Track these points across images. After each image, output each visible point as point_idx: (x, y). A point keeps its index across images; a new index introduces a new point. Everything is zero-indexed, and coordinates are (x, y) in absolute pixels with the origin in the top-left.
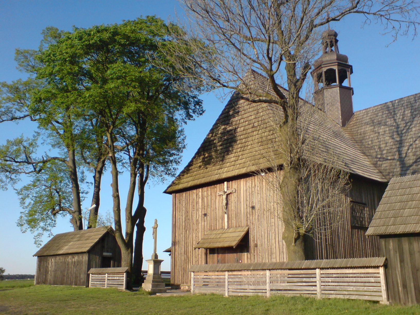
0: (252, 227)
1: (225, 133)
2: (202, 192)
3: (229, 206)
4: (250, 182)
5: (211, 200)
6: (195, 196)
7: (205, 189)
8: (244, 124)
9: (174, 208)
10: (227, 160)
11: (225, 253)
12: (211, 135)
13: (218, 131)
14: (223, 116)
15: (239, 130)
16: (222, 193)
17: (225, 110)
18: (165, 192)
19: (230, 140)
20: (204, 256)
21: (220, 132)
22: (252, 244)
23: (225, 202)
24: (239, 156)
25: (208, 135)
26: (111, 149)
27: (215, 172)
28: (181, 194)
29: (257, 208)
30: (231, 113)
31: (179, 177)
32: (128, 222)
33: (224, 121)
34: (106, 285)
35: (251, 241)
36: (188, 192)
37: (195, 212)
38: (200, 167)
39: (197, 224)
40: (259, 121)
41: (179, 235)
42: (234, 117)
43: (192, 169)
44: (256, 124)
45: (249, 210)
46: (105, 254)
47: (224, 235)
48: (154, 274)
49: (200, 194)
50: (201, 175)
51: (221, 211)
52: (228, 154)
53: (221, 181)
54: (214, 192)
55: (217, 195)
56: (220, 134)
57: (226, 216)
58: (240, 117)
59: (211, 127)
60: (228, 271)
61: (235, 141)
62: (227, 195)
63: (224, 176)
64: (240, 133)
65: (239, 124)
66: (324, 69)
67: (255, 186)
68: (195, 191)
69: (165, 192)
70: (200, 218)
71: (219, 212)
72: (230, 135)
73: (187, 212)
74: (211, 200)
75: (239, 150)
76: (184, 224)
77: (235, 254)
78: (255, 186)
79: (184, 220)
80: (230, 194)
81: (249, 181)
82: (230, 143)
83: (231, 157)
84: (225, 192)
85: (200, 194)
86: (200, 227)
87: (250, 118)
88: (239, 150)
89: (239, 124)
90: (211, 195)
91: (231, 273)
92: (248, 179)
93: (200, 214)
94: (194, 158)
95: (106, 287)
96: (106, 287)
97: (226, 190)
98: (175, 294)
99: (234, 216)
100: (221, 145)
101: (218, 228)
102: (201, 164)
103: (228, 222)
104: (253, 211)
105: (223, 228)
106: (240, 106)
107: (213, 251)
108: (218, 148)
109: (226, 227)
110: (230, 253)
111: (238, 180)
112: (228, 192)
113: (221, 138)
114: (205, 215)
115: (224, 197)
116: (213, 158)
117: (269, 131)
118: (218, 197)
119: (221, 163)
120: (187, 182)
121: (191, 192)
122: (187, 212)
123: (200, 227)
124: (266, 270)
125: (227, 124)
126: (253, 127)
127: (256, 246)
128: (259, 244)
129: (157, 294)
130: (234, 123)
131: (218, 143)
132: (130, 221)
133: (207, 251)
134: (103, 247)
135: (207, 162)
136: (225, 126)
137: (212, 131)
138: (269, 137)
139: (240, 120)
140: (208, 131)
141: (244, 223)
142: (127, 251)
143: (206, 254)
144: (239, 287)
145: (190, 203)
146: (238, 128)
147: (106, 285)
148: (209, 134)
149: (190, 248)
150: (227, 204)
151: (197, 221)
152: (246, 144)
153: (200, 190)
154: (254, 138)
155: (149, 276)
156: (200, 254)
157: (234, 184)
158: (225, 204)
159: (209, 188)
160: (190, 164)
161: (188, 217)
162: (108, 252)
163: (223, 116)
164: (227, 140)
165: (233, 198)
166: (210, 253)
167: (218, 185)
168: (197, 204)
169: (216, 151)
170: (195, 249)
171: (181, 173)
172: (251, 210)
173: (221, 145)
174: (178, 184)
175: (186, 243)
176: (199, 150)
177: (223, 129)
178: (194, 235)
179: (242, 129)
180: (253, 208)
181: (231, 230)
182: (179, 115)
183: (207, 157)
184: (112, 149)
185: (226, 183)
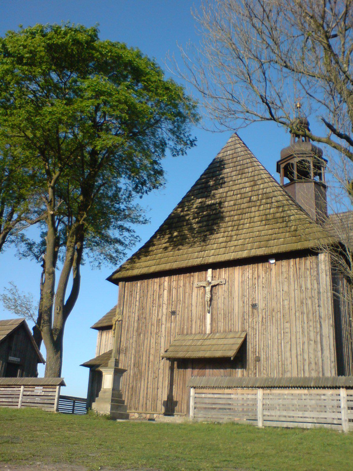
0: (250, 332)
1: (203, 207)
2: (170, 281)
3: (214, 302)
4: (251, 271)
5: (185, 293)
6: (156, 287)
7: (174, 278)
8: (234, 197)
9: (122, 301)
10: (212, 241)
11: (206, 368)
12: (180, 209)
13: (193, 204)
14: (199, 186)
15: (226, 204)
16: (204, 284)
17: (200, 179)
18: (110, 279)
19: (212, 217)
20: (167, 371)
21: (195, 206)
22: (250, 356)
23: (208, 296)
24: (231, 236)
25: (176, 209)
26: (51, 205)
27: (191, 255)
28: (134, 283)
29: (261, 305)
30: (211, 183)
31: (132, 260)
32: (58, 314)
33: (202, 193)
34: (19, 404)
35: (250, 352)
36: (146, 281)
37: (155, 309)
38: (166, 248)
39: (158, 325)
40: (258, 195)
41: (127, 339)
42: (216, 189)
43: (153, 251)
44: (254, 198)
45: (248, 308)
46: (11, 358)
47: (208, 342)
48: (113, 389)
49: (166, 284)
50: (163, 258)
51: (200, 308)
52: (212, 234)
53: (202, 268)
54: (190, 282)
55: (195, 285)
56: (196, 208)
57: (208, 316)
58: (227, 189)
59: (179, 200)
60: (262, 388)
61: (222, 218)
62: (212, 287)
63: (211, 260)
64: (229, 209)
65: (226, 197)
66: (297, 160)
67: (258, 277)
68: (157, 280)
69: (110, 279)
70: (164, 317)
71: (196, 311)
72: (213, 210)
73: (142, 308)
74: (185, 293)
75: (230, 229)
76: (136, 325)
77: (222, 370)
78: (258, 277)
79: (136, 319)
80: (215, 286)
81: (249, 270)
82: (214, 219)
83: (219, 237)
84: (209, 283)
85: (166, 284)
86: (163, 330)
87: (243, 191)
88: (230, 229)
89: (226, 197)
90: (184, 285)
91: (268, 391)
92: (247, 266)
93: (165, 311)
94: (154, 237)
95: (19, 407)
96: (19, 407)
97: (209, 279)
98: (154, 422)
99: (221, 317)
100: (198, 223)
101: (193, 332)
102: (168, 244)
103: (211, 324)
104: (255, 311)
105: (202, 332)
106: (225, 176)
107: (184, 363)
108: (195, 226)
109: (208, 331)
110: (215, 369)
111: (231, 269)
112: (214, 283)
113: (198, 213)
114: (173, 313)
115: (208, 289)
116: (187, 238)
117: (278, 207)
118: (195, 290)
119: (202, 244)
120: (144, 266)
121: (150, 281)
122: (142, 308)
123: (163, 330)
124: (339, 388)
125: (206, 197)
126: (250, 202)
127: (258, 359)
128: (263, 357)
129: (118, 420)
130: (218, 196)
131: (193, 219)
132: (61, 313)
133: (172, 365)
134: (9, 348)
135: (177, 243)
136: (204, 199)
137: (181, 205)
138: (278, 215)
139: (227, 192)
140: (175, 205)
141: (238, 327)
142: (56, 354)
143: (172, 369)
144: (285, 413)
145: (149, 296)
146: (224, 202)
147: (19, 404)
148: (178, 208)
149: (144, 359)
150: (211, 300)
151: (159, 321)
152: (242, 222)
153: (167, 278)
154: (252, 214)
155: (105, 392)
156: (162, 367)
157: (224, 274)
158: (209, 299)
159: (182, 277)
160: (150, 243)
161: (144, 316)
162: (15, 356)
163: (199, 186)
164: (208, 215)
165: (220, 291)
166: (179, 367)
167: (196, 274)
168: (159, 297)
169: (191, 229)
170: (163, 359)
171: (133, 255)
172: (250, 309)
173: (198, 223)
174: (132, 268)
175: (137, 352)
176: (161, 227)
177: (200, 203)
178: (153, 341)
179: (232, 203)
180: (254, 306)
181: (217, 335)
182: (124, 183)
183: (176, 236)
184: (52, 205)
185: (210, 271)
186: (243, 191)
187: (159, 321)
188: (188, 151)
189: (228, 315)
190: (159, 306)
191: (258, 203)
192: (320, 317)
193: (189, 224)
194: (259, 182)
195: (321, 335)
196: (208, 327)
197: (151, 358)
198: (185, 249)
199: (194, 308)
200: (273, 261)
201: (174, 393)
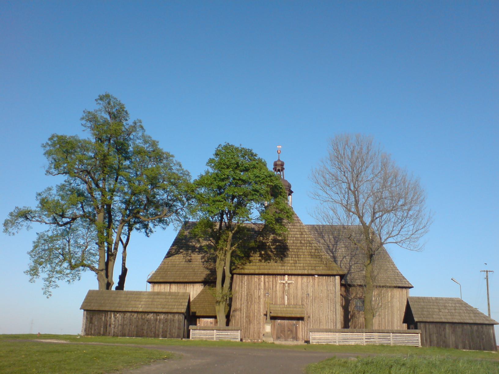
2: (265, 278)
7: (266, 276)
57: (286, 297)
61: (288, 249)
122: (249, 289)
186: (296, 236)
187: (259, 297)
188: (93, 111)
189: (295, 297)
190: (259, 289)
191: (305, 245)
192: (335, 302)
193: (269, 248)
194: (304, 233)
195: (336, 309)
196: (286, 302)
197: (256, 314)
198: (272, 263)
199: (278, 292)
200: (316, 276)
201: (200, 280)
